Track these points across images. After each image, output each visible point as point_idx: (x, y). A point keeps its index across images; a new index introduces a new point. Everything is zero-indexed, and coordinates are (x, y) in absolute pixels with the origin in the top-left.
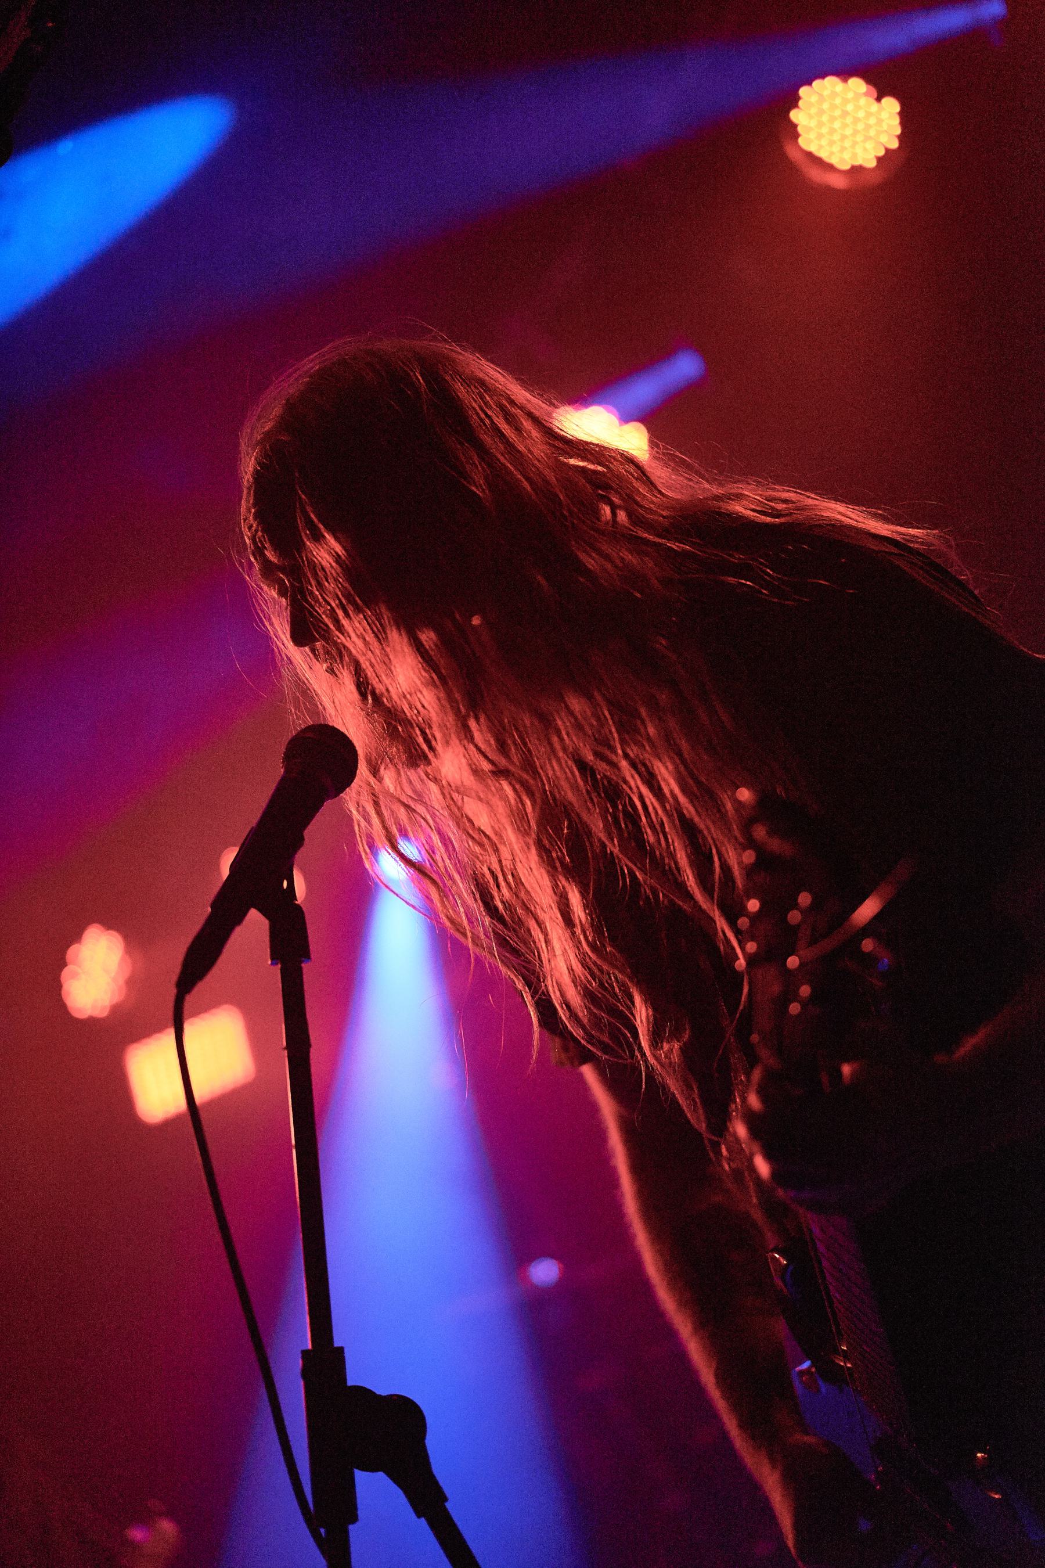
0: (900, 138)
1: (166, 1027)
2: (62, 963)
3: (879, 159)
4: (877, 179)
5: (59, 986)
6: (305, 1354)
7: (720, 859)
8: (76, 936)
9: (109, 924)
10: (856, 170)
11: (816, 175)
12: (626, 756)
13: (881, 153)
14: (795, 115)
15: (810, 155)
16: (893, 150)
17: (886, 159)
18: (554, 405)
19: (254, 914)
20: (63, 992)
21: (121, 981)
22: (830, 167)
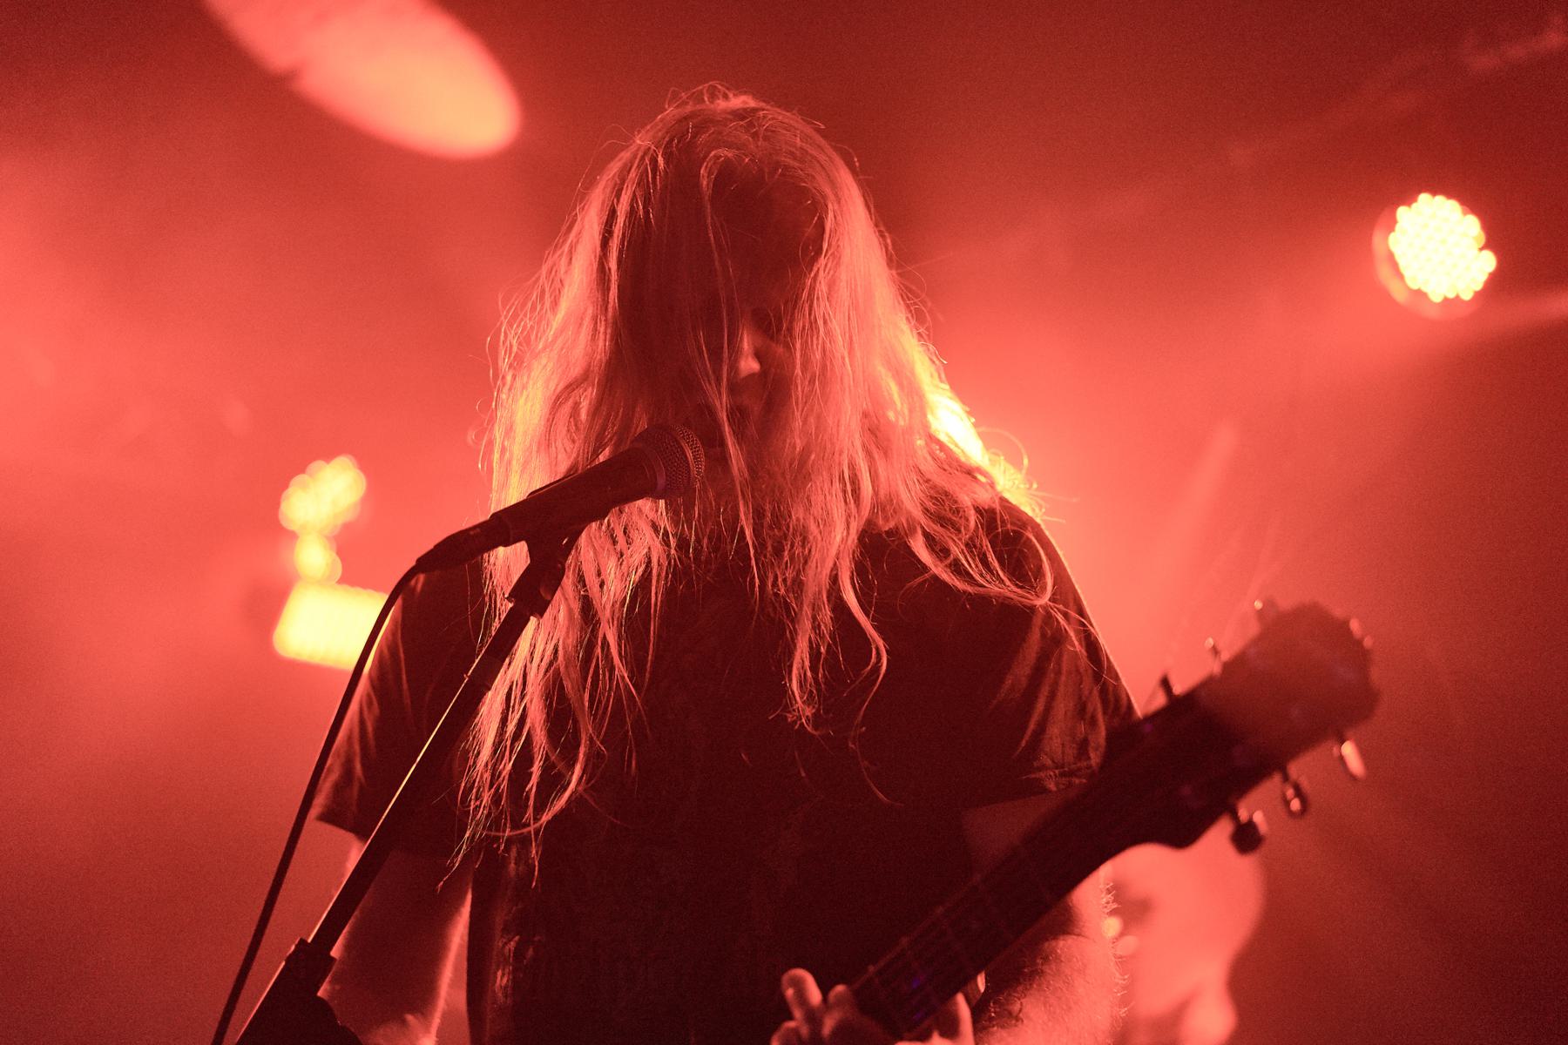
0: (1477, 294)
1: (376, 587)
2: (301, 469)
3: (1446, 300)
4: (1433, 314)
5: (285, 486)
6: (303, 942)
7: (1050, 559)
8: (328, 455)
9: (366, 465)
10: (1420, 295)
11: (1384, 273)
12: (536, 820)
13: (1451, 296)
14: (1402, 212)
15: (1391, 256)
16: (1463, 302)
17: (1451, 303)
18: (1044, 658)
19: (521, 548)
20: (285, 494)
21: (340, 521)
22: (1400, 276)
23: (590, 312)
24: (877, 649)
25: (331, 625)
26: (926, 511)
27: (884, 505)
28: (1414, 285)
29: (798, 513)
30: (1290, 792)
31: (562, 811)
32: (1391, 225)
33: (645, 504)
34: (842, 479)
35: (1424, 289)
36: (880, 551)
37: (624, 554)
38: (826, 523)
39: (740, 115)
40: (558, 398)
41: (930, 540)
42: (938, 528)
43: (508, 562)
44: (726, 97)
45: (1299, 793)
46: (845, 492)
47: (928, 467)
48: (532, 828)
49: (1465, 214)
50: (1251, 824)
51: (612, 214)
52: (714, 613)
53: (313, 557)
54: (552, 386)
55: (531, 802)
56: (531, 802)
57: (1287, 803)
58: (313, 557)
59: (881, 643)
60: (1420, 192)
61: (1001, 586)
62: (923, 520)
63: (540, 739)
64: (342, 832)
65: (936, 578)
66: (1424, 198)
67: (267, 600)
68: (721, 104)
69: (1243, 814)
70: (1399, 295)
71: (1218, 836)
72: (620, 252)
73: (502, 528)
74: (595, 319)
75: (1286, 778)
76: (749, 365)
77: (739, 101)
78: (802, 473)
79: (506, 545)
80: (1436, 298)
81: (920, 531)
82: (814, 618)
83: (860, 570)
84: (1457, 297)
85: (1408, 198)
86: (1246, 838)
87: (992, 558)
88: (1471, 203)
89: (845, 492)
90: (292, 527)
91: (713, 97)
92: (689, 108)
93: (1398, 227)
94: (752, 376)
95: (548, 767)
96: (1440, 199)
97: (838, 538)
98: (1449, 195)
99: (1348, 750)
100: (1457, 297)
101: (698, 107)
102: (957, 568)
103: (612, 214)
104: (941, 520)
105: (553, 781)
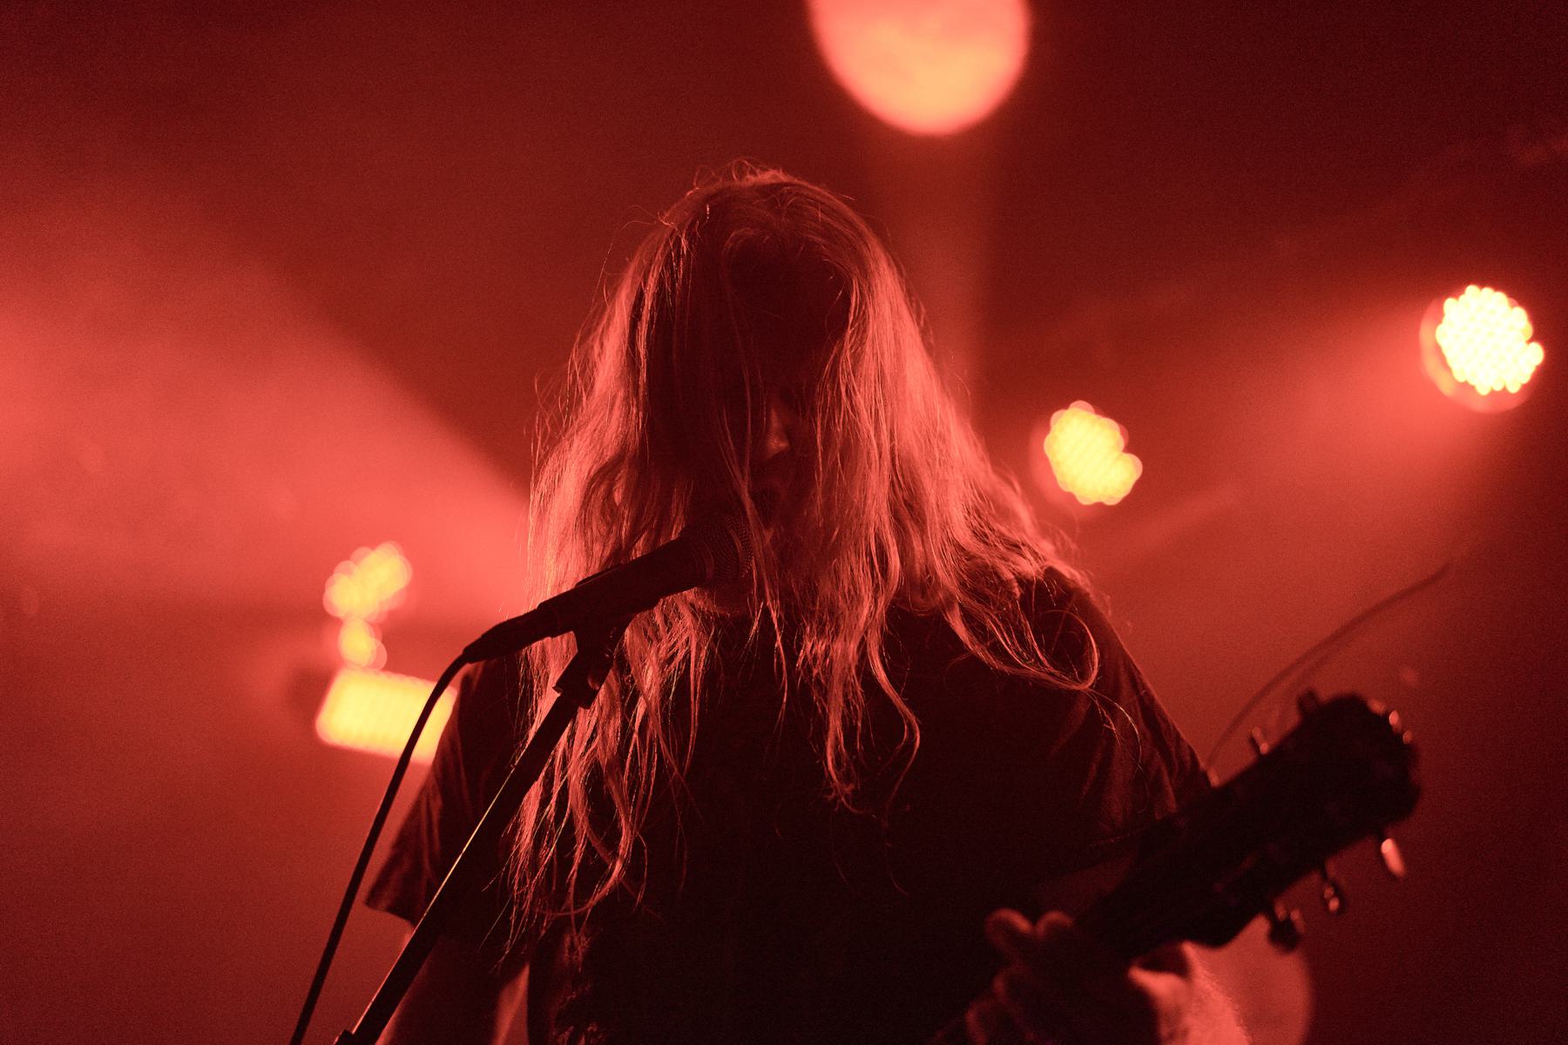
3: (1493, 393)
4: (1480, 407)
10: (1466, 387)
11: (1430, 364)
13: (1498, 388)
14: (1450, 304)
17: (1499, 396)
20: (329, 581)
21: (386, 608)
22: (1447, 368)
23: (621, 394)
24: (910, 725)
25: (379, 713)
26: (963, 584)
27: (918, 583)
28: (1461, 379)
29: (826, 588)
30: (1329, 892)
31: (605, 898)
32: (1439, 317)
33: (690, 594)
34: (869, 554)
35: (1472, 382)
36: (913, 626)
37: (669, 643)
38: (855, 599)
39: (770, 192)
40: (592, 480)
41: (968, 618)
42: (975, 603)
43: (553, 656)
44: (753, 173)
45: (1338, 893)
46: (873, 567)
47: (963, 535)
48: (573, 912)
49: (1513, 306)
50: (1288, 921)
51: (640, 297)
52: (746, 696)
53: (358, 643)
54: (586, 467)
55: (571, 890)
56: (571, 890)
57: (1326, 903)
58: (358, 643)
59: (913, 719)
60: (1469, 283)
61: (1038, 666)
62: (958, 595)
63: (582, 827)
64: (400, 920)
65: (974, 658)
66: (1472, 290)
67: (312, 687)
68: (751, 180)
69: (1281, 912)
70: (1446, 388)
71: (1259, 927)
72: (883, 663)
73: (548, 619)
74: (626, 398)
75: (1325, 877)
76: (776, 444)
77: (768, 176)
78: (830, 551)
79: (553, 635)
80: (1483, 390)
81: (957, 607)
82: (845, 695)
83: (888, 644)
84: (1505, 389)
85: (1455, 289)
86: (1283, 936)
87: (1030, 636)
88: (1519, 295)
89: (873, 567)
90: (340, 614)
91: (741, 175)
92: (719, 185)
93: (1445, 319)
94: (782, 453)
95: (589, 850)
96: (1488, 291)
97: (866, 612)
98: (1496, 288)
99: (1388, 847)
100: (1505, 389)
101: (728, 184)
102: (996, 649)
103: (640, 297)
104: (982, 598)
105: (594, 870)
